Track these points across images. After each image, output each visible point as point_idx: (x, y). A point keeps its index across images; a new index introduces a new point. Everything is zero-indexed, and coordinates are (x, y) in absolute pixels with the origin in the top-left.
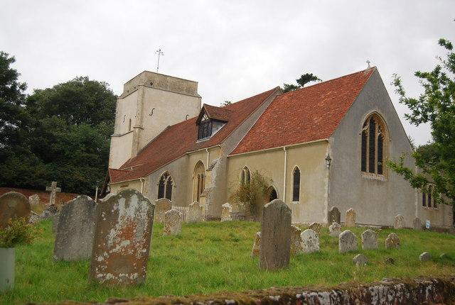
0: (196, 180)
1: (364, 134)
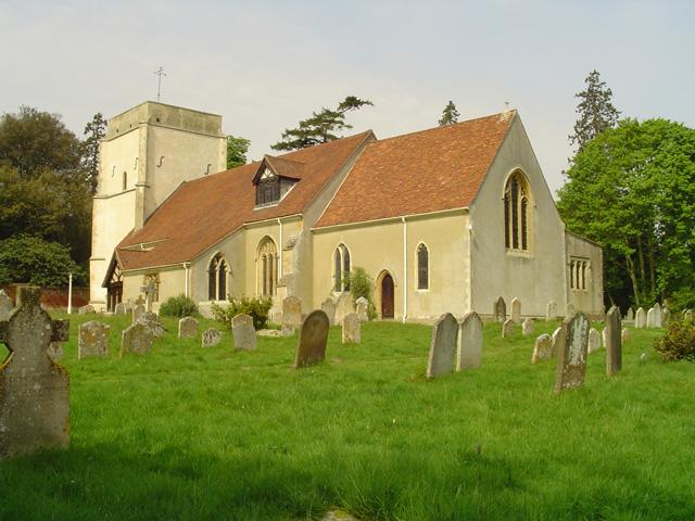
0: (262, 262)
1: (506, 197)
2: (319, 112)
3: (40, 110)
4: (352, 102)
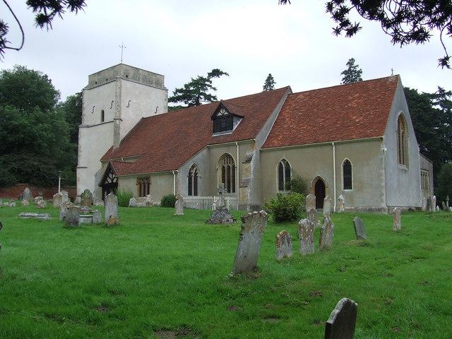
2: (196, 78)
3: (29, 68)
4: (216, 73)
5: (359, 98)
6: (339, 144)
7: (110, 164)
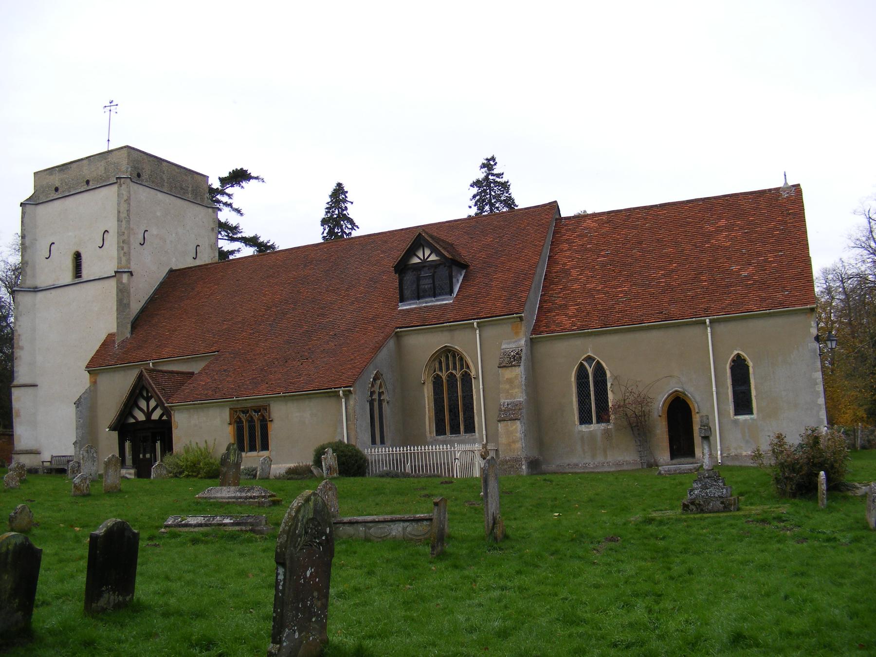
3: (337, 146)
5: (729, 228)
6: (718, 321)
7: (140, 377)
